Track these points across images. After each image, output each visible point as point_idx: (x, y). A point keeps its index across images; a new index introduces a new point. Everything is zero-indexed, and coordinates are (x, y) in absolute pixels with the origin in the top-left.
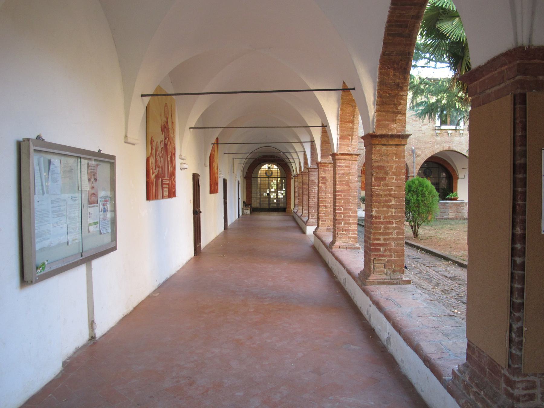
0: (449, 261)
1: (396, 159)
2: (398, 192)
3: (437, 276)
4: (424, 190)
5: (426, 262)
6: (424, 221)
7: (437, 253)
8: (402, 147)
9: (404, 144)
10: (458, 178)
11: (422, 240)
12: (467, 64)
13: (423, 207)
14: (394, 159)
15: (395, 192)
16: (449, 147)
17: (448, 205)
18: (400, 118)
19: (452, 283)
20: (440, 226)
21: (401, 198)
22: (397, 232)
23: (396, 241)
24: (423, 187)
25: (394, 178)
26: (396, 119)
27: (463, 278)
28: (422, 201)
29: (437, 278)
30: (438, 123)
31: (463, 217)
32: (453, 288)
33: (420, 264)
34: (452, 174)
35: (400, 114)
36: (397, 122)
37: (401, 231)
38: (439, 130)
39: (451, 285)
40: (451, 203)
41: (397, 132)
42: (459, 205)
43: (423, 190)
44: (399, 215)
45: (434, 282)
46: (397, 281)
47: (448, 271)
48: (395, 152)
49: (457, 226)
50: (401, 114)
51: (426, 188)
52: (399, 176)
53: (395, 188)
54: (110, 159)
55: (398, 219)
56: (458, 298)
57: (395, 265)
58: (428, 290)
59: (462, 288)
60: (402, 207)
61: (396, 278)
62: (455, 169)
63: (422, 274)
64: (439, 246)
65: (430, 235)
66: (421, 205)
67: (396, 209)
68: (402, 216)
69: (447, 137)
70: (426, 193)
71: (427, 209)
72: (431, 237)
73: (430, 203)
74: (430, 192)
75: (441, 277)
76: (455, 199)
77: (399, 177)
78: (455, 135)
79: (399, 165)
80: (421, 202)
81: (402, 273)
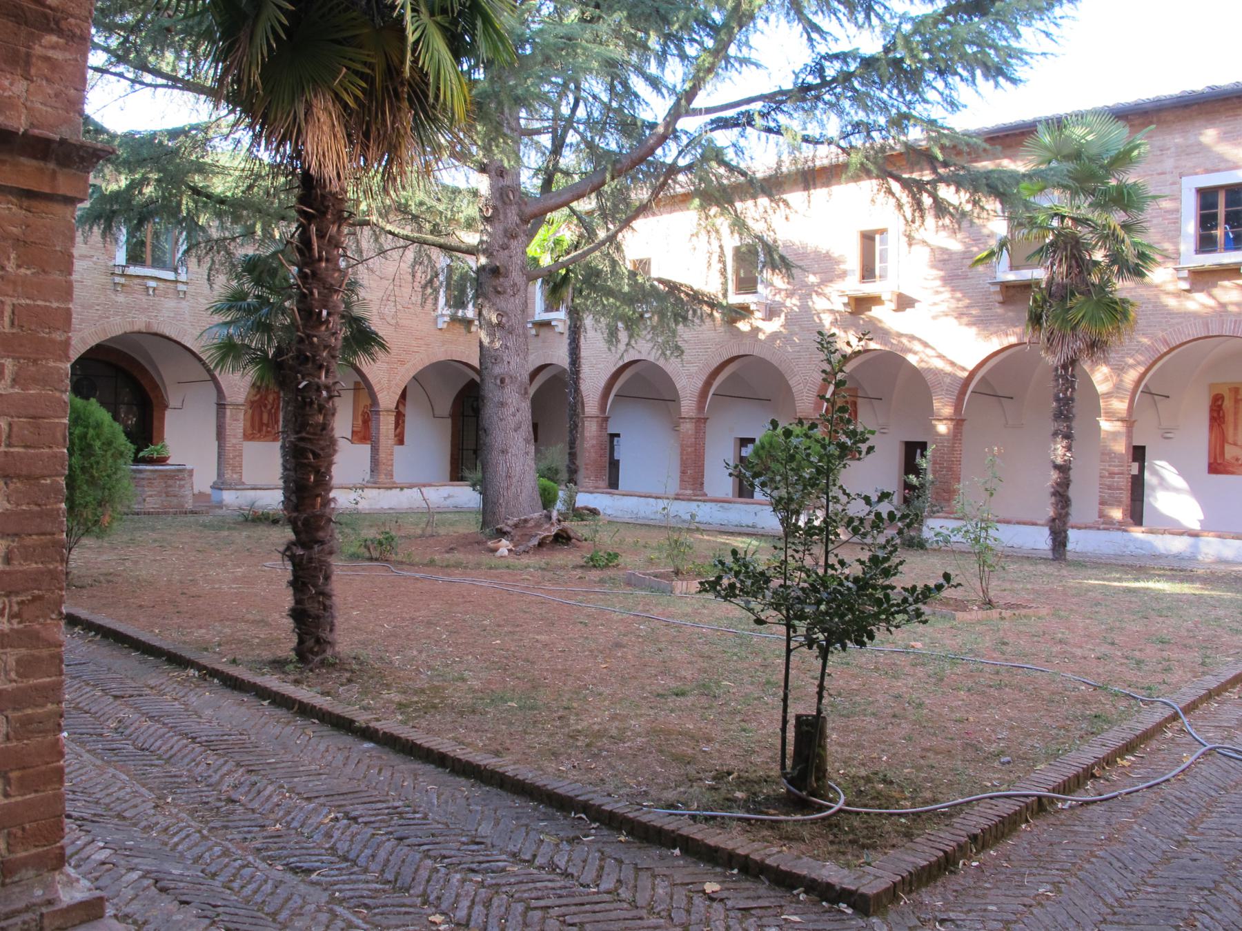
0: (186, 668)
1: (23, 271)
2: (26, 447)
3: (161, 737)
4: (89, 436)
5: (110, 676)
6: (88, 531)
7: (143, 639)
8: (58, 209)
9: (69, 194)
10: (166, 407)
11: (82, 587)
12: (273, 28)
13: (85, 487)
14: (11, 267)
15: (9, 445)
16: (148, 325)
17: (141, 476)
18: (57, 55)
19: (225, 769)
20: (126, 538)
21: (44, 477)
22: (18, 662)
23: (14, 709)
24: (87, 427)
25: (6, 371)
26: (28, 55)
27: (253, 738)
28: (83, 469)
29: (164, 748)
30: (121, 256)
31: (183, 506)
32: (235, 796)
33: (88, 689)
34: (152, 395)
35: (51, 31)
36: (33, 71)
37: (45, 653)
38: (123, 275)
39: (223, 777)
40: (152, 471)
41: (32, 125)
42: (172, 477)
43: (87, 433)
44: (34, 565)
45: (155, 770)
46: (24, 923)
47: (196, 713)
48: (14, 230)
49: (172, 535)
50: (60, 32)
51: (95, 428)
52: (35, 361)
53: (10, 425)
54: (1171, 579)
55: (27, 590)
56: (267, 849)
57: (9, 834)
58: (144, 823)
59: (267, 793)
60: (48, 527)
61: (21, 905)
62: (159, 383)
63: (101, 735)
64: (141, 606)
65: (103, 571)
66: (79, 482)
67: (16, 535)
68: (50, 571)
69: (144, 298)
70: (97, 444)
71: (100, 493)
72: (109, 578)
73: (109, 476)
74: (109, 443)
75: (177, 742)
76: (162, 460)
77: (33, 369)
78: (165, 295)
79: (40, 303)
80: (78, 472)
81: (54, 869)
